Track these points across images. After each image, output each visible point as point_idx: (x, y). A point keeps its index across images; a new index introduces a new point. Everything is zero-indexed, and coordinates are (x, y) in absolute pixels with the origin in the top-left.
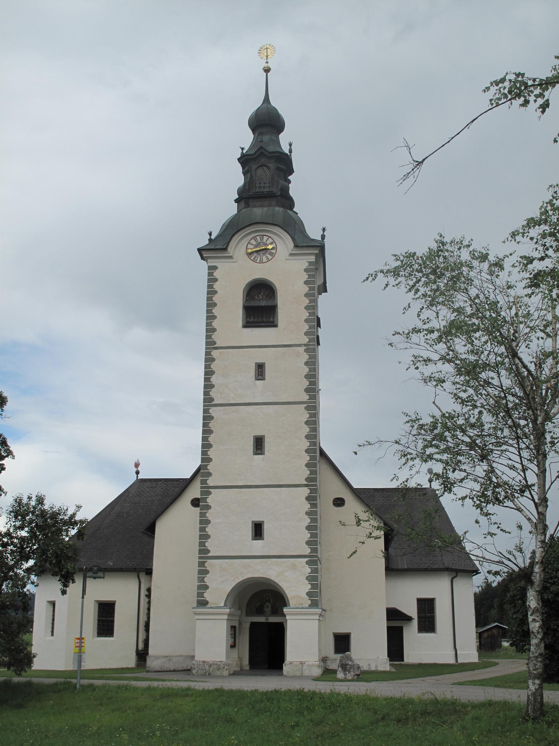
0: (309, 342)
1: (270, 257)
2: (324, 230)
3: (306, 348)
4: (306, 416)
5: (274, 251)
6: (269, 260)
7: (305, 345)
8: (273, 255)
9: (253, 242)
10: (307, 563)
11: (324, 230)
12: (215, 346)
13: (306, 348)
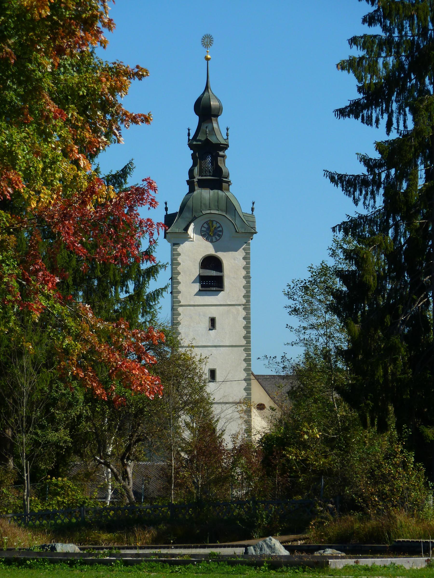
0: (246, 302)
1: (218, 238)
2: (253, 203)
3: (244, 307)
4: (244, 355)
5: (221, 233)
6: (217, 240)
7: (243, 305)
8: (220, 236)
9: (206, 226)
10: (244, 350)
11: (253, 203)
12: (180, 304)
13: (244, 307)
